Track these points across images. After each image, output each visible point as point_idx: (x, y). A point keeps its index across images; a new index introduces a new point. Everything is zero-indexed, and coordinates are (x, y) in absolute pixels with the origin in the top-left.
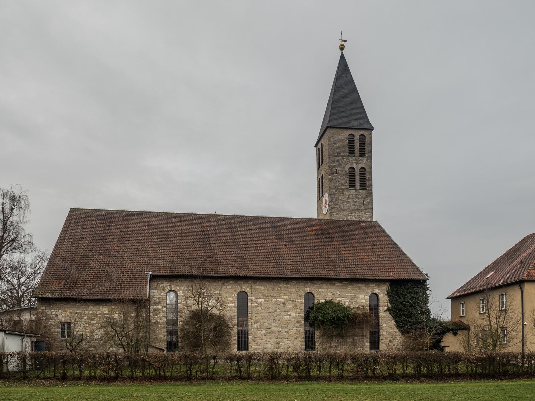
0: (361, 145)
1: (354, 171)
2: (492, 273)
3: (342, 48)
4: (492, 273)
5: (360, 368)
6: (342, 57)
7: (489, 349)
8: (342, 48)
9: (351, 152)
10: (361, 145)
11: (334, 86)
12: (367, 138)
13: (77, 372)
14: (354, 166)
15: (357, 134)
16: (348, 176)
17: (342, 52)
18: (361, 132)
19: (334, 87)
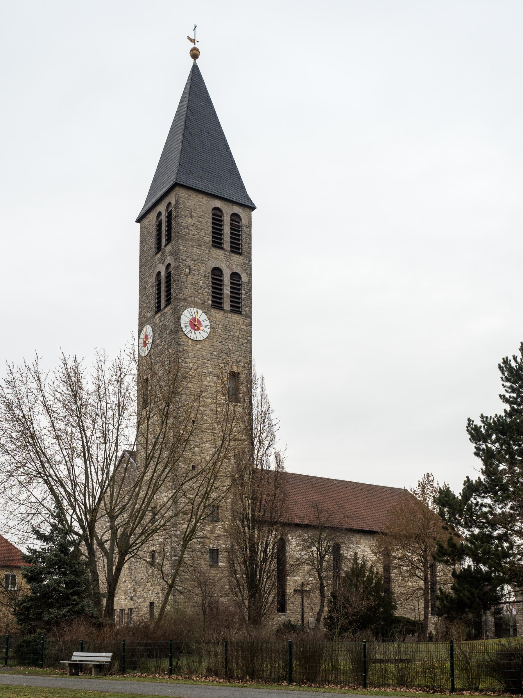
0: (215, 300)
1: (221, 277)
2: (114, 571)
3: (195, 54)
4: (114, 571)
5: (40, 634)
6: (195, 74)
7: (26, 537)
8: (195, 54)
9: (217, 243)
10: (215, 300)
11: (189, 85)
12: (244, 222)
13: (131, 555)
14: (223, 266)
15: (228, 210)
16: (210, 297)
17: (195, 62)
18: (237, 210)
19: (187, 99)
